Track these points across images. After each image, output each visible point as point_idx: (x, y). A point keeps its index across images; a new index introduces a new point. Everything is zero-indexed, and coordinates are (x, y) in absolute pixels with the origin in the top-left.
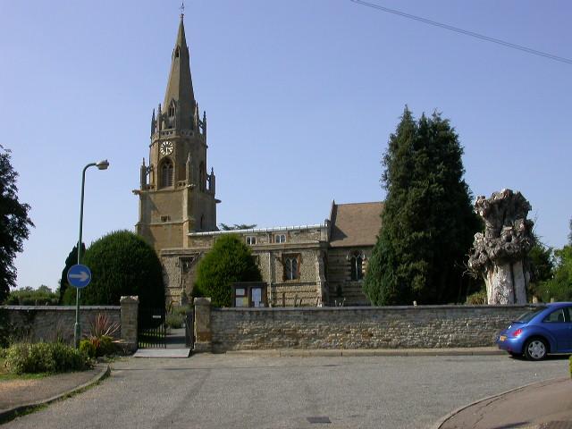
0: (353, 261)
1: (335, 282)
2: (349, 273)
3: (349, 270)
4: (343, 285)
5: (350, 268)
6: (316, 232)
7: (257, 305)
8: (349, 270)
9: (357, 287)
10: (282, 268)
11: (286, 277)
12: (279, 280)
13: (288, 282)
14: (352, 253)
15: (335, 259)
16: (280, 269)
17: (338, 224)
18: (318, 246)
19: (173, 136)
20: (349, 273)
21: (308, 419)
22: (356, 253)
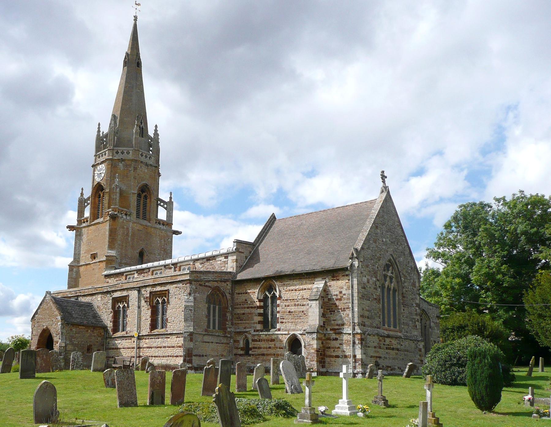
0: (264, 300)
1: (240, 333)
2: (260, 318)
3: (260, 315)
4: (250, 337)
5: (261, 311)
6: (223, 259)
7: (253, 343)
8: (260, 315)
9: (268, 340)
10: (149, 312)
11: (154, 326)
12: (145, 330)
13: (156, 332)
14: (262, 291)
15: (243, 298)
16: (147, 313)
17: (262, 249)
18: (187, 277)
19: (106, 157)
20: (260, 318)
21: (543, 389)
22: (271, 288)
